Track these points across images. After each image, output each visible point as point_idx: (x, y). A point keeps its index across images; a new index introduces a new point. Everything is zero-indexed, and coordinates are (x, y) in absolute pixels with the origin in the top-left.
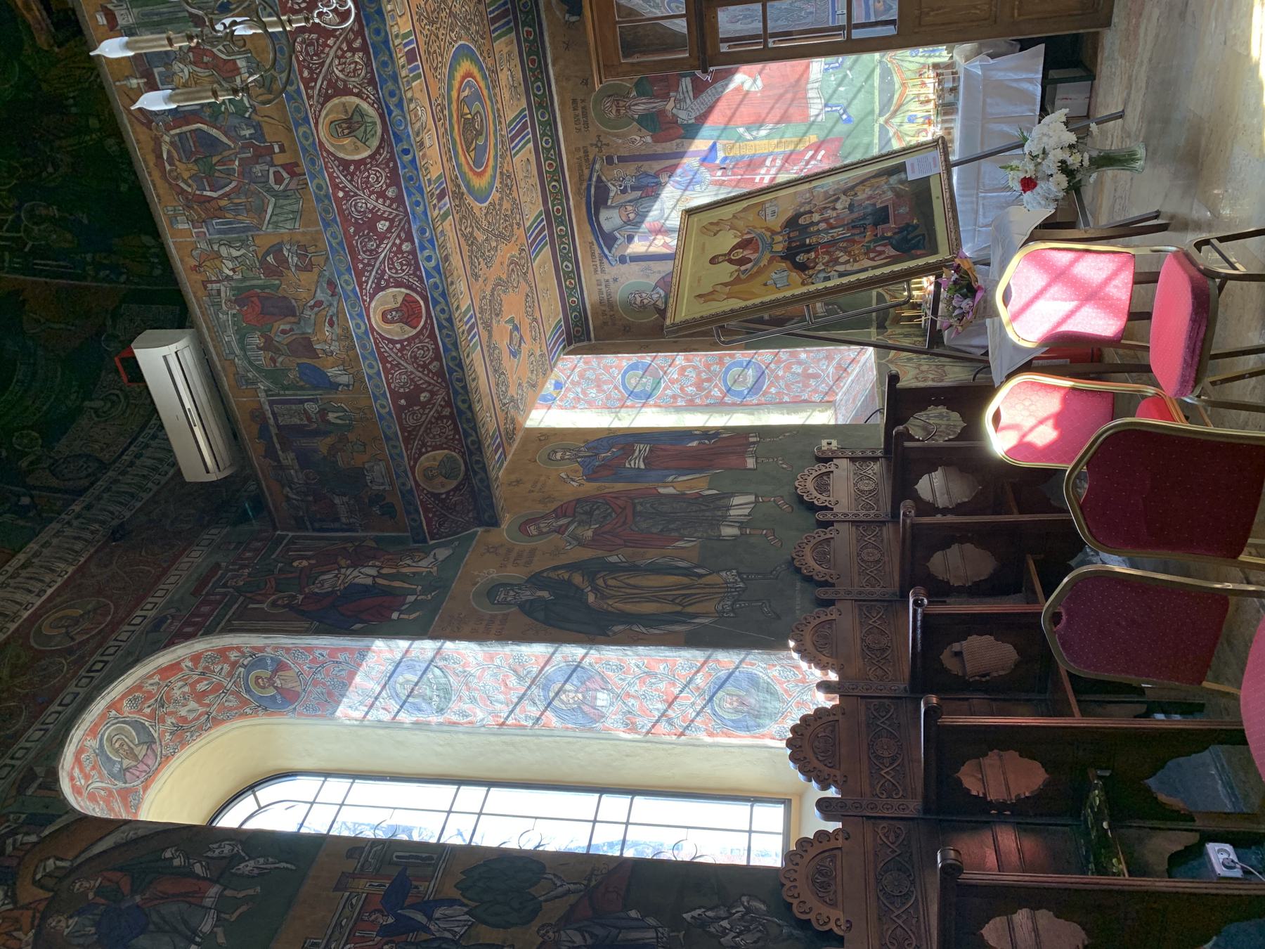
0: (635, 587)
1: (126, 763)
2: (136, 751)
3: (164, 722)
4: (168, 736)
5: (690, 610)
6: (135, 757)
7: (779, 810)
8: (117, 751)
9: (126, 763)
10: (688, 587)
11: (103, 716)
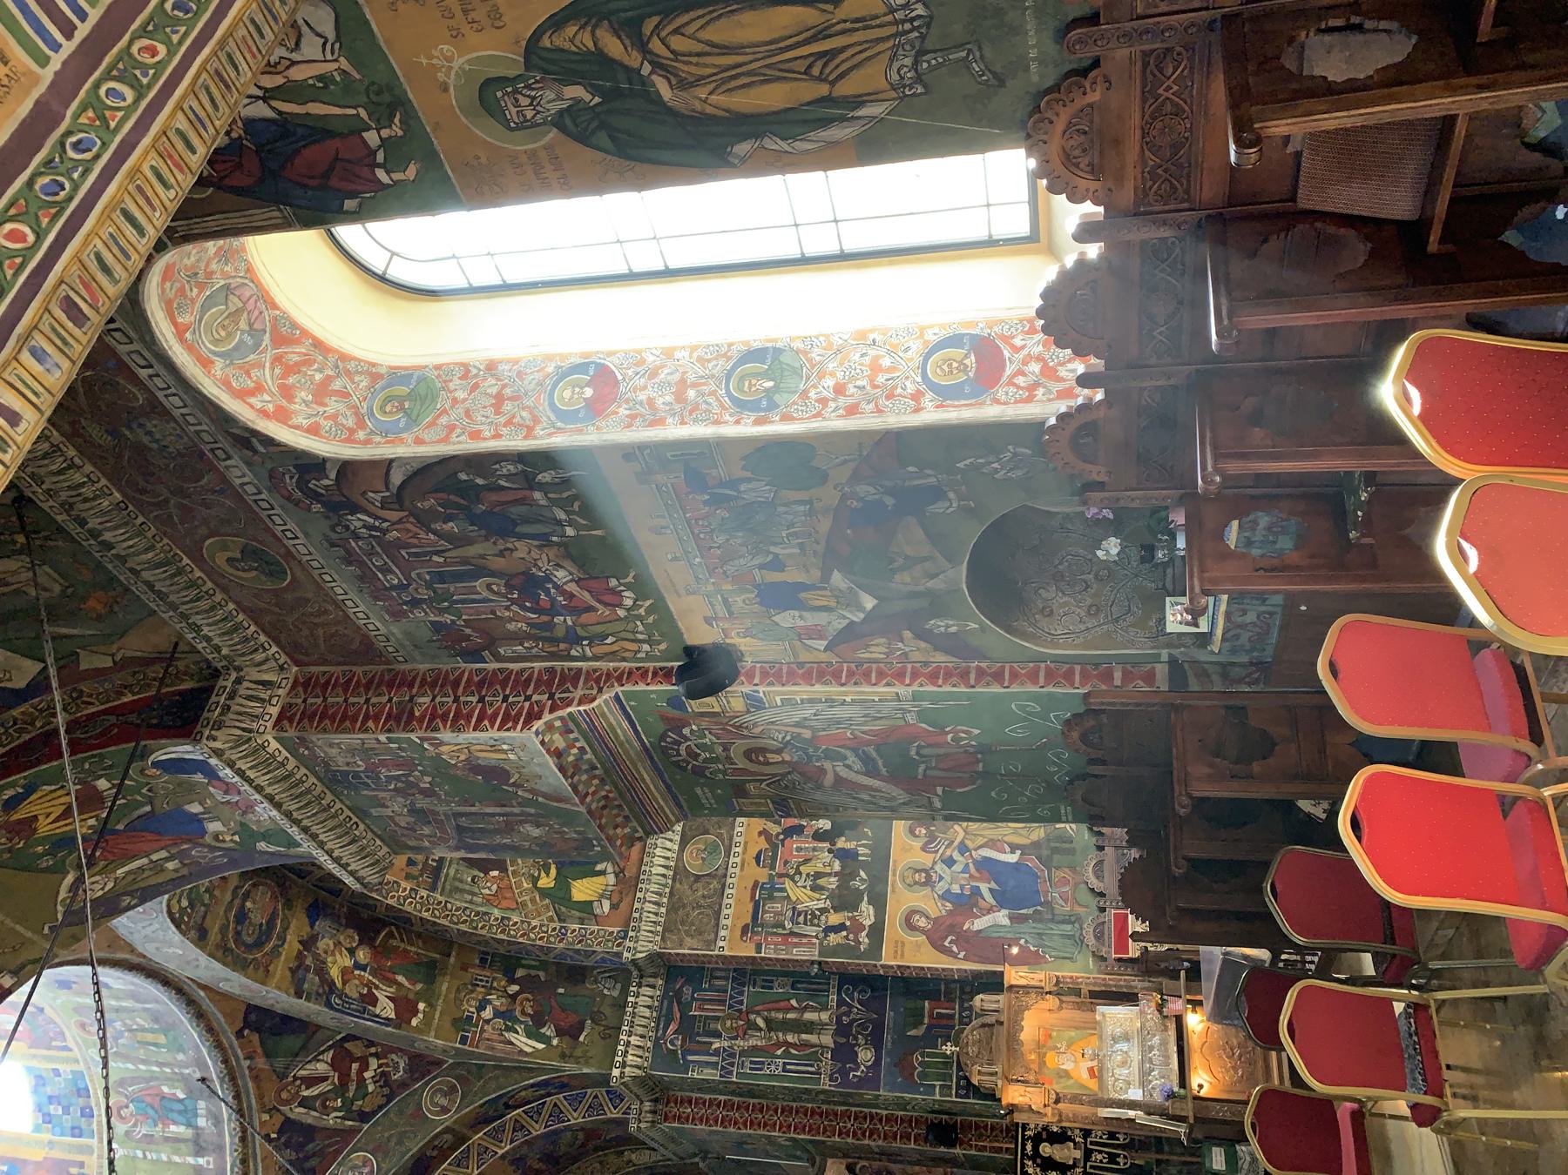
0: (726, 49)
1: (243, 325)
2: (232, 309)
3: (212, 273)
4: (227, 268)
5: (845, 89)
6: (238, 312)
7: (1024, 229)
8: (229, 335)
9: (243, 325)
10: (822, 34)
11: (190, 348)
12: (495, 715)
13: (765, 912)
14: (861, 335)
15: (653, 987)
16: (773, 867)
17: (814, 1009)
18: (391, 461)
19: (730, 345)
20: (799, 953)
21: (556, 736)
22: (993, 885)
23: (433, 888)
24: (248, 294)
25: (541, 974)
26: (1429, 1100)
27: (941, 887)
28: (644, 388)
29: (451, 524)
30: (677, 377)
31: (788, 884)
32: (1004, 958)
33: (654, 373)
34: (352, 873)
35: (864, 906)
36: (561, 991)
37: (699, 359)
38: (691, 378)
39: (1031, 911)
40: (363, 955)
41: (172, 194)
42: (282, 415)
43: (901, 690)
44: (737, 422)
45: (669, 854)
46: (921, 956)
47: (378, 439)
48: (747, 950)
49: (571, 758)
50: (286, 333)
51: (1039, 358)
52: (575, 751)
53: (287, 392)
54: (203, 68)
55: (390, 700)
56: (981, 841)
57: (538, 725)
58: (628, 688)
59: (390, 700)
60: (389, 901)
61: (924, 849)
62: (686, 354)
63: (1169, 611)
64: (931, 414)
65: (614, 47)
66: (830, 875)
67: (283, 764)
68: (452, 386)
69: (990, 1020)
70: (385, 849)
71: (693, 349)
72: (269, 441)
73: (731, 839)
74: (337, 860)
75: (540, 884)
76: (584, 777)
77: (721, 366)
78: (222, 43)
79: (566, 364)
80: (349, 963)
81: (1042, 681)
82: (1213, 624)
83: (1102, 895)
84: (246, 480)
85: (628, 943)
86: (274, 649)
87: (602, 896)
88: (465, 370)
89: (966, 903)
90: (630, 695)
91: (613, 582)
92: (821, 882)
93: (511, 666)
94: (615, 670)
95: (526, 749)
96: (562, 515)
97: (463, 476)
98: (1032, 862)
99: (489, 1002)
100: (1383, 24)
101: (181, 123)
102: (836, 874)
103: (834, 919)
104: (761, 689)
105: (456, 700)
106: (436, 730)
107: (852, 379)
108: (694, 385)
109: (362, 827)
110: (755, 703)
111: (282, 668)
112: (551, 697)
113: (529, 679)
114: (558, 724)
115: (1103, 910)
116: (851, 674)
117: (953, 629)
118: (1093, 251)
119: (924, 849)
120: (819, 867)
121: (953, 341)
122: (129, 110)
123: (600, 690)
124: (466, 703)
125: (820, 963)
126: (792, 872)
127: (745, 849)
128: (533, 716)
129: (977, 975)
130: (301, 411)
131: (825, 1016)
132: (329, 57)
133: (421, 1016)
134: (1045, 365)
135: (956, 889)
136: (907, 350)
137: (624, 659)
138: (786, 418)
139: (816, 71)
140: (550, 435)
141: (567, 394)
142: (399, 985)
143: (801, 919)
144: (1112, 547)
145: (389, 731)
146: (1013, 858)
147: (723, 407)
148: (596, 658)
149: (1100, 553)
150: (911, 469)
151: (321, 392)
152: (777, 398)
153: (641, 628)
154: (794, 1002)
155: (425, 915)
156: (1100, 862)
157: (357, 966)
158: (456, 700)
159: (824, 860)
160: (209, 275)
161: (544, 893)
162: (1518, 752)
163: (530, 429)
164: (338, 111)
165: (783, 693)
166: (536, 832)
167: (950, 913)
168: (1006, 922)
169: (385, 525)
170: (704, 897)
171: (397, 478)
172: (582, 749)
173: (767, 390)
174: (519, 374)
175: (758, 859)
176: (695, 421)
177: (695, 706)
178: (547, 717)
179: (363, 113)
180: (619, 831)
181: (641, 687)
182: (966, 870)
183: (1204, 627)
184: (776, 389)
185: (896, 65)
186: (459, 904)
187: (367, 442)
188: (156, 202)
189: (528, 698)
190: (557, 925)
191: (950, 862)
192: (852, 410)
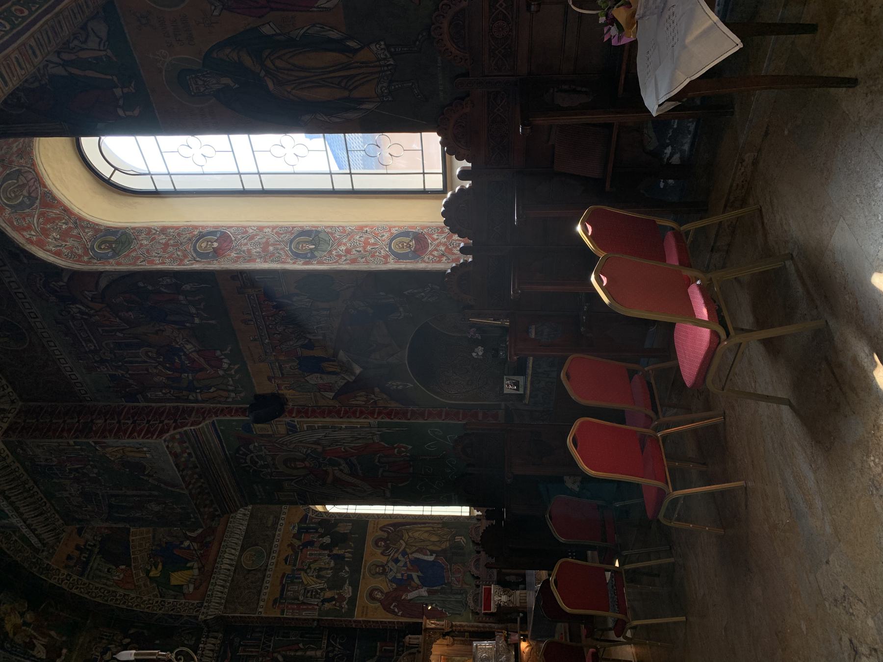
1: (25, 193)
3: (13, 161)
6: (24, 185)
8: (17, 197)
12: (141, 430)
13: (288, 591)
14: (361, 228)
15: (216, 638)
16: (295, 565)
17: (313, 649)
18: (101, 273)
19: (293, 228)
20: (305, 615)
21: (176, 444)
22: (420, 574)
23: (82, 575)
24: (30, 177)
25: (145, 631)
26: (620, 616)
27: (391, 575)
28: (246, 244)
29: (130, 313)
30: (264, 240)
31: (303, 574)
32: (423, 613)
33: (252, 238)
34: (37, 536)
35: (346, 587)
36: (157, 642)
37: (277, 233)
38: (271, 241)
39: (439, 588)
40: (29, 617)
41: (23, 72)
42: (41, 244)
43: (371, 420)
44: (294, 263)
45: (233, 557)
46: (378, 615)
47: (95, 261)
48: (275, 613)
49: (183, 459)
50: (49, 200)
51: (444, 244)
52: (186, 455)
53: (45, 232)
54: (46, 23)
55: (79, 421)
56: (414, 549)
57: (167, 436)
58: (221, 418)
59: (78, 421)
60: (52, 581)
61: (382, 554)
62: (270, 230)
63: (506, 382)
64: (392, 265)
65: (247, 61)
66: (327, 569)
67: (4, 459)
68: (140, 238)
69: (413, 650)
70: (61, 521)
71: (274, 228)
72: (31, 257)
73: (271, 549)
74: (29, 526)
75: (151, 574)
76: (190, 472)
77: (288, 237)
78: (57, 15)
79: (205, 231)
80: (19, 621)
81: (443, 417)
82: (525, 388)
83: (478, 578)
84: (12, 279)
85: (203, 610)
86: (10, 389)
87: (190, 582)
88: (149, 231)
89: (404, 584)
90: (219, 421)
91: (218, 353)
92: (323, 573)
93: (153, 404)
94: (214, 408)
95: (158, 450)
96: (193, 311)
97: (141, 284)
98: (442, 560)
99: (109, 649)
100: (584, 89)
101: (32, 42)
102: (331, 569)
103: (328, 594)
104: (296, 420)
105: (119, 422)
106: (105, 437)
107: (355, 247)
108: (273, 245)
109: (48, 505)
110: (292, 429)
111: (13, 402)
112: (175, 421)
113: (163, 412)
114: (178, 436)
115: (478, 586)
116: (346, 412)
117: (400, 387)
118: (467, 184)
119: (382, 554)
120: (322, 565)
121: (405, 234)
122: (7, 33)
123: (204, 419)
124: (124, 424)
125: (318, 620)
126: (306, 567)
127: (279, 555)
128: (162, 432)
129: (408, 625)
130: (51, 241)
131: (319, 653)
132: (102, 48)
133: (63, 657)
134: (447, 247)
135: (399, 576)
136: (382, 236)
137: (220, 402)
138: (319, 263)
139: (343, 84)
140: (192, 264)
141: (204, 245)
142: (50, 636)
143: (309, 594)
144: (480, 351)
145: (76, 438)
146: (431, 558)
147: (287, 256)
148: (203, 401)
149: (474, 354)
150: (382, 293)
151: (65, 235)
152: (316, 253)
153: (231, 383)
154: (301, 645)
155: (74, 591)
156: (478, 560)
157: (25, 624)
158: (119, 422)
159: (325, 561)
160: (11, 162)
161: (152, 579)
162: (647, 415)
163: (181, 260)
164: (103, 76)
165: (307, 422)
166: (156, 508)
167: (395, 590)
168: (425, 594)
169: (92, 312)
170: (252, 582)
171: (103, 283)
172: (189, 454)
173: (311, 249)
174: (179, 234)
175: (286, 560)
176: (272, 261)
177: (258, 428)
178: (172, 432)
179: (115, 79)
180: (206, 509)
181: (228, 418)
182: (405, 565)
183: (521, 392)
184: (316, 249)
185: (380, 86)
186: (97, 585)
187: (88, 263)
188: (15, 73)
189: (161, 422)
190: (160, 599)
191: (397, 561)
192: (354, 261)
